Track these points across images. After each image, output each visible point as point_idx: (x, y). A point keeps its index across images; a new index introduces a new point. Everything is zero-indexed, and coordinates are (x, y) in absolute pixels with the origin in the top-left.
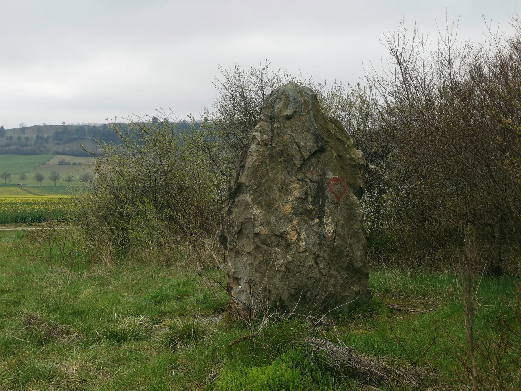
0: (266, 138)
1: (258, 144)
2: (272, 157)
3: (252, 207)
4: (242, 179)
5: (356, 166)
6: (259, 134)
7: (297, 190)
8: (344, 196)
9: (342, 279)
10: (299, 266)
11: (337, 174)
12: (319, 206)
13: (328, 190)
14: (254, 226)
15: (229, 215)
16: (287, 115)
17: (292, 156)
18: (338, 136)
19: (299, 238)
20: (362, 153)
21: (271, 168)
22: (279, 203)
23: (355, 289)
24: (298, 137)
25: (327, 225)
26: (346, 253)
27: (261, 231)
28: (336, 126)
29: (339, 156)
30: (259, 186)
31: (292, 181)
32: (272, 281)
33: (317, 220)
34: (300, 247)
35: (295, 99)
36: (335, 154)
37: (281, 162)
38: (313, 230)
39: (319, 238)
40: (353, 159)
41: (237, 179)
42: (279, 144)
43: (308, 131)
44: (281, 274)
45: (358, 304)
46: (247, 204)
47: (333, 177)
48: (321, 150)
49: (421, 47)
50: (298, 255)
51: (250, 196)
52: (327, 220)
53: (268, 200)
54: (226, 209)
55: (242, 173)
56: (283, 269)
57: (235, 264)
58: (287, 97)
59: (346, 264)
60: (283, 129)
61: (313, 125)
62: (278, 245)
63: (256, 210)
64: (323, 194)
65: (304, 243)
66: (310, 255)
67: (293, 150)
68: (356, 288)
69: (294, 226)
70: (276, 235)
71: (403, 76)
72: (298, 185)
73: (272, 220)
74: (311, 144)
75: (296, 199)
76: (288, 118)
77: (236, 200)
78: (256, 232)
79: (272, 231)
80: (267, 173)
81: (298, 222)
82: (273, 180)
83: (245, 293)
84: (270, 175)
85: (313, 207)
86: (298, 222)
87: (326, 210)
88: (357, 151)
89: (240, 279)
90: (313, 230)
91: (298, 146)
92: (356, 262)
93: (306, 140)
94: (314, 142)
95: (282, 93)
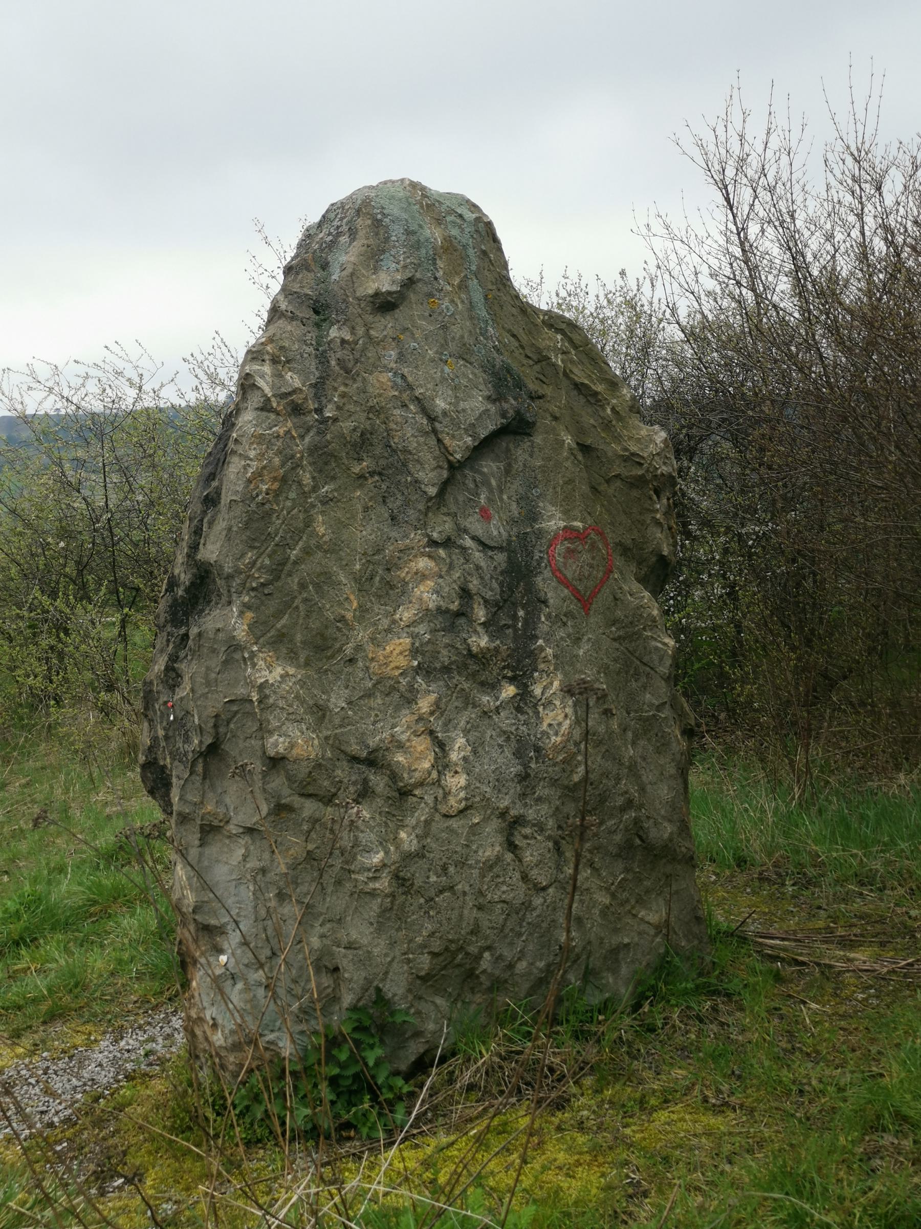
0: (297, 383)
1: (265, 407)
2: (323, 458)
3: (253, 655)
4: (209, 547)
5: (647, 484)
6: (267, 369)
7: (430, 583)
8: (606, 591)
9: (607, 889)
10: (445, 868)
11: (576, 512)
12: (516, 638)
13: (547, 573)
14: (263, 730)
15: (173, 688)
16: (377, 294)
17: (406, 451)
18: (580, 375)
19: (442, 764)
20: (663, 434)
21: (324, 503)
22: (362, 634)
23: (653, 918)
24: (423, 379)
25: (549, 704)
26: (620, 801)
27: (292, 746)
28: (571, 341)
29: (585, 449)
30: (278, 571)
31: (408, 548)
32: (342, 935)
33: (509, 691)
34: (446, 794)
35: (409, 232)
36: (568, 440)
37: (361, 477)
38: (494, 726)
39: (518, 754)
40: (632, 459)
41: (194, 547)
42: (351, 407)
43: (464, 355)
44: (375, 906)
45: (663, 968)
46: (234, 647)
47: (562, 524)
48: (517, 428)
49: (785, 159)
50: (439, 824)
51: (241, 614)
52: (545, 688)
53: (315, 625)
54: (160, 666)
55: (211, 524)
56: (383, 884)
57: (199, 874)
58: (377, 224)
59: (618, 838)
60: (364, 349)
61: (484, 332)
62: (365, 793)
63: (270, 667)
64: (530, 589)
65: (462, 780)
66: (486, 819)
67: (407, 429)
68: (654, 914)
69: (420, 719)
70: (354, 759)
71: (739, 238)
72: (431, 564)
73: (337, 701)
74: (476, 403)
75: (427, 614)
76: (385, 304)
77: (194, 631)
78: (272, 753)
79: (336, 745)
80: (308, 522)
81: (437, 704)
82: (333, 549)
83: (240, 986)
84: (321, 530)
85: (490, 641)
86: (439, 699)
87: (542, 649)
88: (644, 430)
89: (221, 930)
90: (494, 726)
91: (424, 411)
92: (655, 824)
93: (455, 388)
94: (488, 398)
95: (358, 211)
